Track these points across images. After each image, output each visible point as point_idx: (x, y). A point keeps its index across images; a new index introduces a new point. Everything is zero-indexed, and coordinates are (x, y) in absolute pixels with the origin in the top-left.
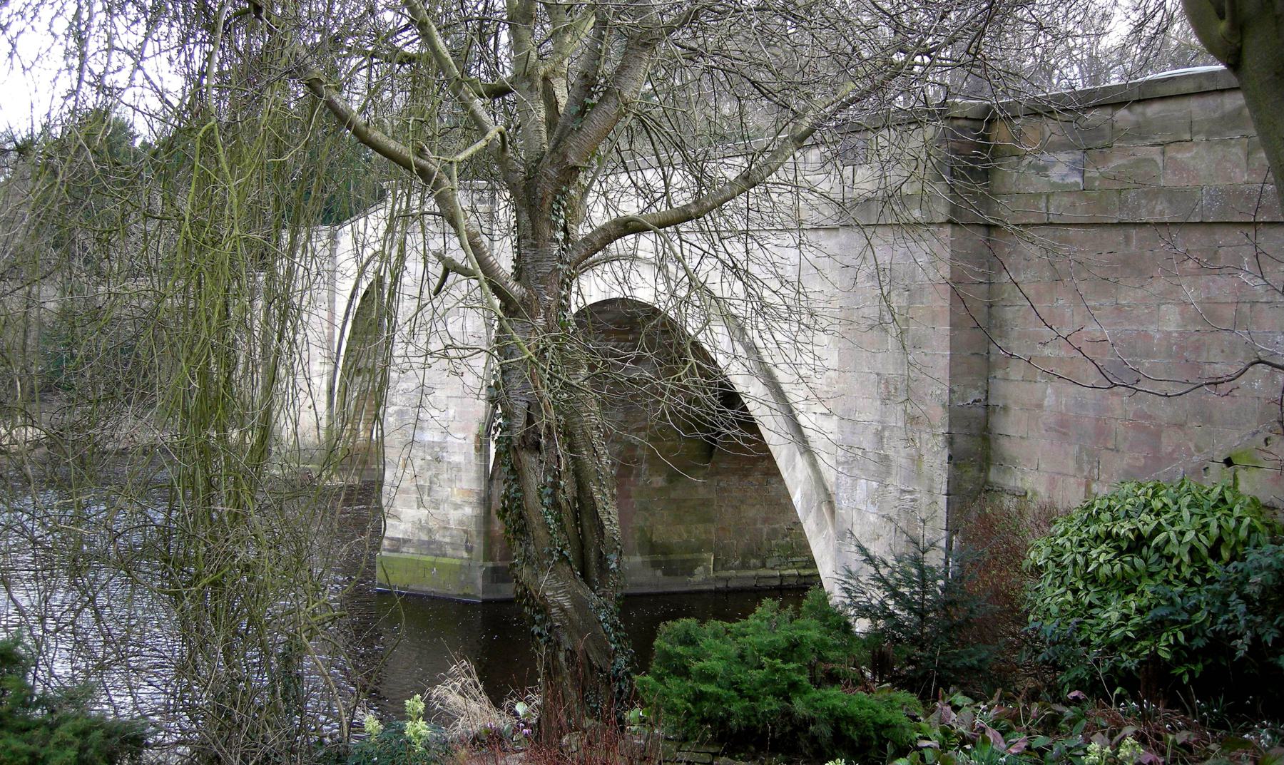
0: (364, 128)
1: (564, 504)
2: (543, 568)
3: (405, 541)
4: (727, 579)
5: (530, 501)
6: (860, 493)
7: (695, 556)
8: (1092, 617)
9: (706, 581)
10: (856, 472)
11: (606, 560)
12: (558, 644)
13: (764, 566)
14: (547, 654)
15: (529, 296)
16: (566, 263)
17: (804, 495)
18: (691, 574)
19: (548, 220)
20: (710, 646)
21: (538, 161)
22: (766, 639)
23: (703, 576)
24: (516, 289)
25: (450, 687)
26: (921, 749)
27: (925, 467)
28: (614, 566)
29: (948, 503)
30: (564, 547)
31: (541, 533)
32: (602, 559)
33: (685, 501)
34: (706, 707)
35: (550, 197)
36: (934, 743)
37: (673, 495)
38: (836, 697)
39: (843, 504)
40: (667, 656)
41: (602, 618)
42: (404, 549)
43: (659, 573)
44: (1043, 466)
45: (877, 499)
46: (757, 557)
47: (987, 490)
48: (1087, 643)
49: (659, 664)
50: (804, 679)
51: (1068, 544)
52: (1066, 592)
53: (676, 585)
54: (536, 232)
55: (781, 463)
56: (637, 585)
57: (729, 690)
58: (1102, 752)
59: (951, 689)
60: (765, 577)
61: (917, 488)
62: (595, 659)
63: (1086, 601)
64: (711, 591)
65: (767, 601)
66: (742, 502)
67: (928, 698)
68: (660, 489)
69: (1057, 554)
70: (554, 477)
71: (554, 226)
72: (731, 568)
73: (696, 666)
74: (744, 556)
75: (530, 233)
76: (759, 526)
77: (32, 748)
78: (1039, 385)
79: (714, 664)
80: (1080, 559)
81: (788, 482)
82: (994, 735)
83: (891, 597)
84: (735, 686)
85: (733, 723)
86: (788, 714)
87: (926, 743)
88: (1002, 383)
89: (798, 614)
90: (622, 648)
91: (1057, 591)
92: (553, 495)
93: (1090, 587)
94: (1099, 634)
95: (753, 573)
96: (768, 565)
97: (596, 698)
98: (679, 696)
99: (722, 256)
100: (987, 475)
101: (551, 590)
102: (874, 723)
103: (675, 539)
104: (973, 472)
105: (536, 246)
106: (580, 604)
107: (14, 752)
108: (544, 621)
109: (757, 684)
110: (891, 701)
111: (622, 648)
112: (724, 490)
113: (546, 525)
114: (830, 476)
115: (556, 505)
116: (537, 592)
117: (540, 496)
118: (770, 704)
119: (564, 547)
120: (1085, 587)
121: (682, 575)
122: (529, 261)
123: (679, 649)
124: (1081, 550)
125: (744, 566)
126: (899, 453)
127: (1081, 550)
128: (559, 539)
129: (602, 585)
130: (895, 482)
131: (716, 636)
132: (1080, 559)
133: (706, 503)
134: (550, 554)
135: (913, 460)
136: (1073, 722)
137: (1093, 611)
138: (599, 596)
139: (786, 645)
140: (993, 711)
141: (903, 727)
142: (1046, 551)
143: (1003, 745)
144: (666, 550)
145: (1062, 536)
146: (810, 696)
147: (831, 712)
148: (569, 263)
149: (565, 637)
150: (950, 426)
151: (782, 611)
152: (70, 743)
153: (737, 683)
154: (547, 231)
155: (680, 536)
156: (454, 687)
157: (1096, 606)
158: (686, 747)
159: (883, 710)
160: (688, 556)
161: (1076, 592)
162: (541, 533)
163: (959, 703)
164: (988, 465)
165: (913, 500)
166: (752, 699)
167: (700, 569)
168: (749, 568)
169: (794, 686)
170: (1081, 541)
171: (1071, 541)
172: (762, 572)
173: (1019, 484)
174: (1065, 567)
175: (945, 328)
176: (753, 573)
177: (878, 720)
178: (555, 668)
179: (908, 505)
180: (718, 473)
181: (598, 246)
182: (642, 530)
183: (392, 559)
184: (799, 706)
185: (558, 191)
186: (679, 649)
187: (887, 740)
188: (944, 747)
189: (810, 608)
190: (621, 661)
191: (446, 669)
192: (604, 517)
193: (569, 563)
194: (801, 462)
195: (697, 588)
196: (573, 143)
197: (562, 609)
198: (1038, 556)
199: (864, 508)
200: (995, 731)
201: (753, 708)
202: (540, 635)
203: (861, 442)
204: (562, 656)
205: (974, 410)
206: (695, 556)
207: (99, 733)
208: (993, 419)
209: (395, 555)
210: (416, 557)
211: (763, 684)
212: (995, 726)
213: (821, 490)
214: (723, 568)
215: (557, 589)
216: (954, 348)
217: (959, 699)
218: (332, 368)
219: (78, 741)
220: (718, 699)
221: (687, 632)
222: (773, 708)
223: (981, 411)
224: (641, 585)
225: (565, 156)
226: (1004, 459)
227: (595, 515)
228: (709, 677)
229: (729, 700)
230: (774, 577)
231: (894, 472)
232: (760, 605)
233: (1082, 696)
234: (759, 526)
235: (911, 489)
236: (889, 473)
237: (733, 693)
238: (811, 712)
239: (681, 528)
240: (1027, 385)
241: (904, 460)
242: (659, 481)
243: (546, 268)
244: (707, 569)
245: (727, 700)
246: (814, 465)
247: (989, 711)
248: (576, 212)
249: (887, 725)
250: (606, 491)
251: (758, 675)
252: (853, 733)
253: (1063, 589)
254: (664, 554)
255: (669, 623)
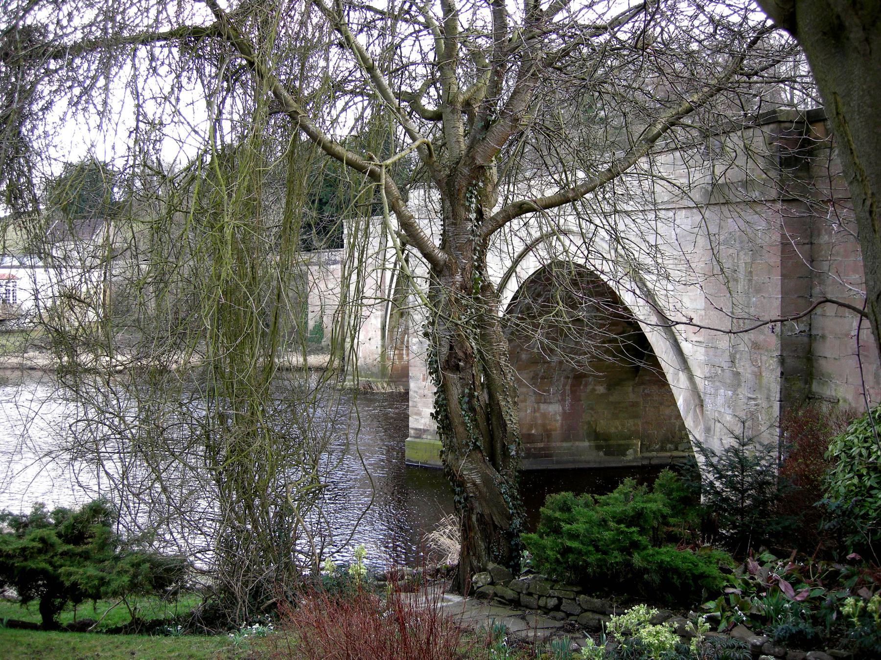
0: (329, 145)
1: (478, 409)
2: (462, 455)
3: (425, 431)
4: (650, 459)
5: (452, 406)
6: (720, 400)
7: (626, 442)
8: (871, 496)
9: (635, 459)
10: (717, 384)
11: (508, 449)
12: (472, 509)
13: (676, 449)
14: (464, 517)
15: (450, 260)
16: (477, 235)
17: (685, 400)
18: (625, 455)
19: (463, 205)
20: (579, 513)
21: (457, 163)
22: (619, 509)
23: (633, 456)
24: (441, 255)
25: (442, 533)
26: (727, 594)
27: (765, 381)
28: (513, 453)
29: (781, 407)
30: (477, 440)
31: (461, 429)
32: (505, 450)
33: (619, 403)
34: (571, 557)
35: (464, 188)
36: (738, 591)
37: (611, 399)
38: (668, 554)
39: (709, 406)
40: (549, 519)
41: (503, 491)
42: (424, 436)
43: (601, 453)
44: (850, 380)
45: (731, 403)
46: (671, 442)
47: (810, 397)
48: (865, 516)
49: (544, 525)
50: (644, 540)
51: (856, 441)
52: (853, 477)
53: (613, 462)
54: (455, 215)
55: (670, 378)
56: (585, 462)
57: (588, 546)
58: (856, 605)
59: (761, 549)
60: (677, 457)
61: (759, 396)
62: (497, 520)
63: (868, 484)
64: (638, 467)
65: (627, 480)
66: (661, 404)
67: (740, 558)
68: (602, 395)
69: (848, 447)
70: (470, 389)
71: (468, 210)
72: (653, 451)
73: (566, 527)
74: (662, 443)
75: (451, 214)
76: (673, 421)
77: (101, 574)
78: (846, 320)
79: (580, 527)
80: (864, 452)
81: (675, 391)
82: (786, 586)
83: (717, 479)
84: (594, 543)
85: (590, 570)
86: (628, 564)
87: (731, 590)
88: (821, 317)
89: (651, 490)
90: (518, 513)
91: (847, 476)
92: (469, 402)
93: (873, 475)
94: (875, 510)
95: (669, 454)
96: (680, 448)
97: (498, 549)
98: (552, 549)
99: (606, 227)
100: (810, 387)
101: (467, 470)
102: (692, 574)
103: (613, 430)
104: (800, 384)
105: (455, 224)
106: (487, 481)
107: (88, 577)
108: (462, 492)
109: (609, 542)
110: (709, 557)
111: (518, 513)
112: (648, 395)
113: (464, 424)
114: (701, 384)
115: (472, 409)
116: (457, 471)
117: (460, 403)
118: (616, 557)
119: (477, 440)
120: (868, 474)
121: (618, 455)
122: (450, 234)
123: (558, 514)
124: (866, 445)
125: (662, 449)
126: (746, 369)
127: (866, 445)
128: (474, 433)
129: (505, 467)
130: (744, 392)
131: (587, 505)
132: (864, 452)
133: (635, 404)
134: (467, 445)
135: (756, 376)
136: (847, 577)
137: (873, 492)
138: (502, 475)
139: (632, 514)
140: (787, 567)
141: (715, 578)
142: (840, 444)
143: (793, 594)
144: (606, 437)
145: (852, 434)
146: (645, 552)
147: (660, 564)
148: (479, 236)
149: (477, 504)
150: (782, 350)
151: (639, 487)
152: (126, 572)
153: (595, 541)
154: (462, 212)
155: (616, 428)
156: (444, 533)
157: (874, 488)
158: (557, 587)
159: (700, 564)
160: (622, 442)
161: (860, 476)
162: (461, 429)
163: (765, 559)
164: (812, 379)
165: (756, 405)
166: (605, 553)
167: (631, 451)
168: (666, 451)
169: (635, 545)
170: (866, 438)
171: (858, 438)
172: (675, 453)
173: (834, 394)
174: (853, 458)
175: (777, 278)
176: (669, 454)
177: (696, 572)
178: (469, 527)
179: (753, 408)
180: (643, 383)
181: (501, 223)
182: (589, 423)
183: (415, 443)
184: (637, 559)
185: (470, 184)
186: (558, 514)
187: (702, 587)
188: (745, 593)
189: (660, 485)
190: (517, 522)
191: (439, 519)
192: (507, 418)
193: (481, 451)
194: (683, 377)
195: (628, 464)
196: (479, 149)
197: (474, 484)
198: (834, 450)
199: (723, 410)
200: (786, 583)
201: (604, 560)
202: (459, 502)
203: (720, 363)
204: (474, 518)
205: (799, 338)
206: (626, 442)
207: (148, 565)
208: (815, 345)
209: (418, 440)
210: (432, 442)
211: (613, 542)
212: (787, 578)
213: (696, 397)
214: (648, 450)
215: (472, 469)
216: (785, 293)
217: (767, 556)
218: (384, 313)
219: (132, 571)
220: (579, 552)
221: (565, 502)
222: (617, 560)
223: (806, 339)
224: (588, 462)
225: (474, 159)
226: (823, 375)
227: (500, 417)
228: (573, 536)
229: (588, 553)
230: (684, 457)
231: (743, 384)
232: (622, 483)
233: (858, 557)
234: (673, 421)
235: (754, 396)
236: (739, 385)
237: (591, 548)
238: (645, 564)
239: (617, 423)
240: (838, 320)
241: (750, 376)
242: (601, 389)
243: (463, 240)
244: (636, 451)
245: (586, 554)
246: (691, 377)
247: (784, 567)
248: (485, 199)
249: (702, 576)
250: (509, 399)
251: (607, 535)
252: (676, 580)
253: (851, 475)
254: (605, 440)
255: (553, 495)
